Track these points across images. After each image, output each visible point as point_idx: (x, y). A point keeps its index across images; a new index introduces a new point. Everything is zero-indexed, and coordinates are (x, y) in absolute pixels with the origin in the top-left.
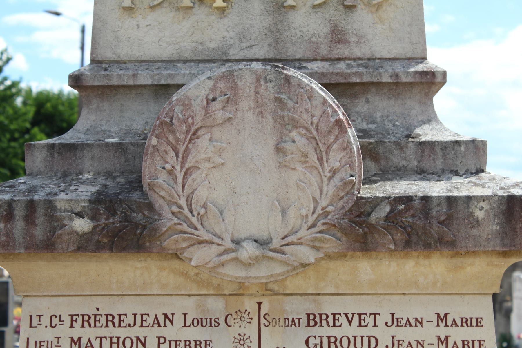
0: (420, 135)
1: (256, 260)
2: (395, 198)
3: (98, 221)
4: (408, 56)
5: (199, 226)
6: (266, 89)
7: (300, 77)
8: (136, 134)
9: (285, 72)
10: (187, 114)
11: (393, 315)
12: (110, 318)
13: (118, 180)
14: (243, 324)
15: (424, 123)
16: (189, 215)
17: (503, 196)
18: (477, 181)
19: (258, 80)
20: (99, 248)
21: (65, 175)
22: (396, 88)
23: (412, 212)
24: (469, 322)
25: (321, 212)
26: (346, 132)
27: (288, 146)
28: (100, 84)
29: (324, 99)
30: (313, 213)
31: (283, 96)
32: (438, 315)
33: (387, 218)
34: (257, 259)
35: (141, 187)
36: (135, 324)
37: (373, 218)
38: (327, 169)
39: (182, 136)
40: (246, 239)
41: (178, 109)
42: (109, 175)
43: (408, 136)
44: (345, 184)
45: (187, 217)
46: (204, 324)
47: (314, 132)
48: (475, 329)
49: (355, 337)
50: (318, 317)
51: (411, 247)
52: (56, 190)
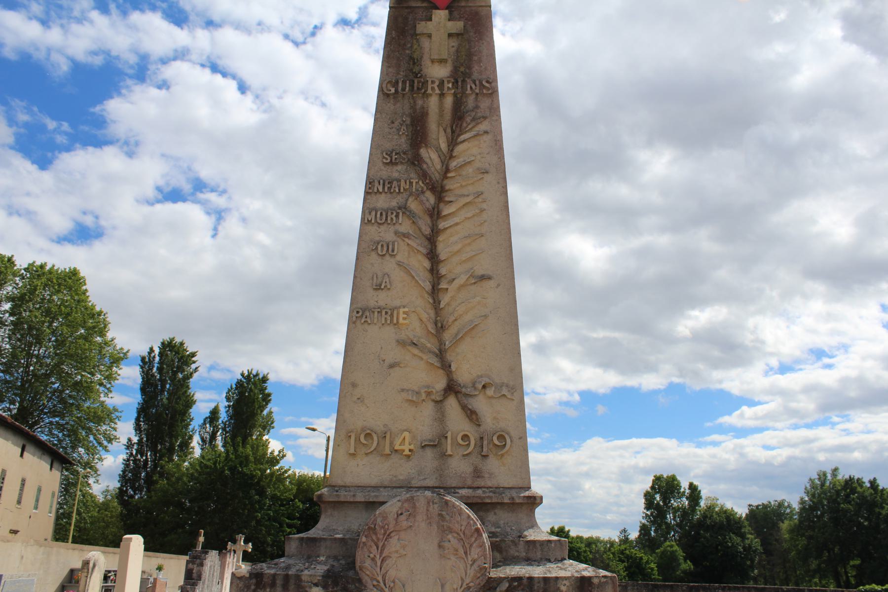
19: (428, 503)
21: (309, 557)
22: (513, 506)
27: (446, 544)
31: (444, 513)
35: (354, 568)
38: (470, 559)
39: (381, 537)
41: (379, 520)
42: (336, 558)
43: (520, 537)
44: (481, 569)
52: (303, 568)
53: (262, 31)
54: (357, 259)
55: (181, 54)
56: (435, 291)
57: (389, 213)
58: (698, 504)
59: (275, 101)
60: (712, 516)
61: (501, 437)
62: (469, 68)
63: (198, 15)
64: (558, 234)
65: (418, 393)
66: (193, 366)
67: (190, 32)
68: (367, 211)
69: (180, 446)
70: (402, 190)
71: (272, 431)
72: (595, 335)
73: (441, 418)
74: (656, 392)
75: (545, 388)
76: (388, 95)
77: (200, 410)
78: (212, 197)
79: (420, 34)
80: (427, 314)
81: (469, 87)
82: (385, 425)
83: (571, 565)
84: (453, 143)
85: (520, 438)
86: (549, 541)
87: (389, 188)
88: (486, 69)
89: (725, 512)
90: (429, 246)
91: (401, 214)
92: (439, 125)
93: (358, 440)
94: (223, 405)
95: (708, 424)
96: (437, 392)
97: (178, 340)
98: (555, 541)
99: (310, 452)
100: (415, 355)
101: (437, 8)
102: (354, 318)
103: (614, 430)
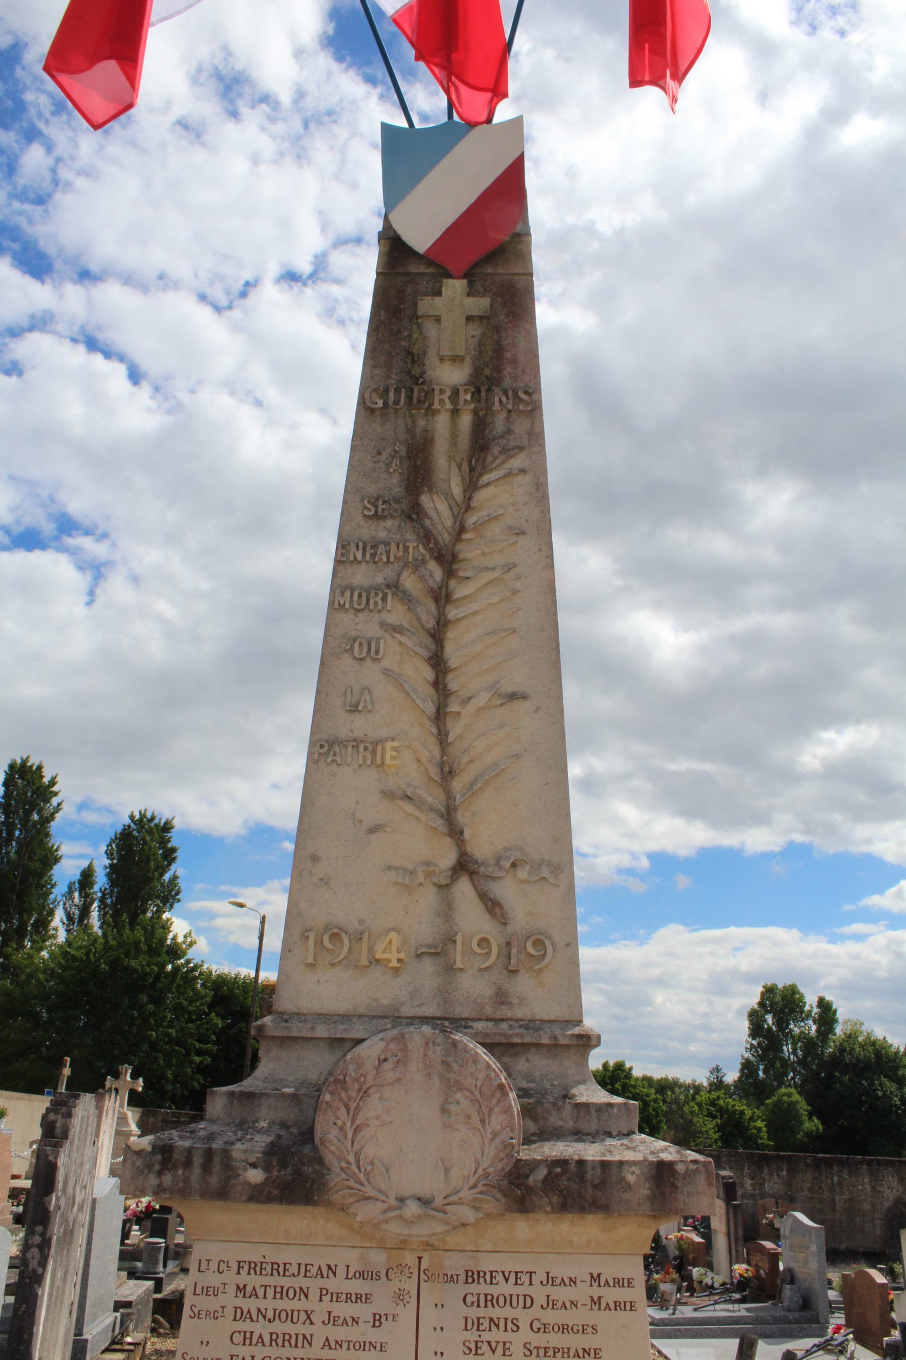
0: (576, 1096)
1: (418, 1219)
2: (552, 1161)
3: (270, 1172)
4: (566, 1019)
5: (365, 1183)
6: (434, 1052)
7: (465, 1041)
8: (310, 1084)
9: (453, 1036)
10: (360, 1072)
11: (548, 1273)
12: (275, 1266)
13: (291, 1130)
14: (403, 1278)
15: (580, 1083)
16: (357, 1171)
17: (653, 1162)
18: (629, 1144)
19: (427, 1043)
20: (269, 1199)
23: (568, 1175)
24: (621, 1283)
25: (482, 1173)
26: (507, 1095)
27: (453, 1108)
28: (280, 1034)
29: (488, 1063)
30: (475, 1173)
31: (450, 1060)
32: (592, 1275)
33: (545, 1180)
34: (419, 1217)
35: (313, 1139)
36: (299, 1274)
37: (531, 1181)
38: (489, 1131)
39: (354, 1094)
40: (409, 1197)
41: (351, 1067)
43: (565, 1097)
44: (506, 1147)
45: (354, 1173)
46: (366, 1277)
47: (478, 1095)
48: (628, 1312)
49: (511, 1296)
50: (476, 1273)
51: (567, 1210)
52: (233, 1139)
53: (166, 288)
54: (322, 664)
55: (40, 322)
56: (440, 716)
57: (372, 594)
58: (831, 1030)
59: (184, 397)
60: (852, 1049)
61: (539, 943)
62: (498, 369)
63: (66, 262)
64: (628, 615)
65: (412, 873)
66: (55, 801)
67: (55, 287)
68: (338, 591)
69: (36, 926)
70: (392, 559)
71: (176, 905)
72: (673, 767)
73: (447, 912)
74: (766, 857)
75: (596, 847)
76: (372, 411)
77: (66, 871)
78: (87, 543)
79: (422, 317)
80: (430, 750)
81: (497, 399)
82: (361, 921)
83: (643, 1142)
84: (471, 486)
85: (568, 945)
86: (610, 1105)
87: (373, 555)
88: (523, 372)
89: (874, 1043)
90: (433, 647)
91: (390, 596)
92: (451, 458)
93: (319, 942)
94: (101, 865)
95: (848, 907)
96: (441, 872)
97: (34, 761)
98: (619, 1105)
99: (233, 939)
100: (408, 815)
101: (450, 276)
102: (316, 755)
103: (702, 913)
